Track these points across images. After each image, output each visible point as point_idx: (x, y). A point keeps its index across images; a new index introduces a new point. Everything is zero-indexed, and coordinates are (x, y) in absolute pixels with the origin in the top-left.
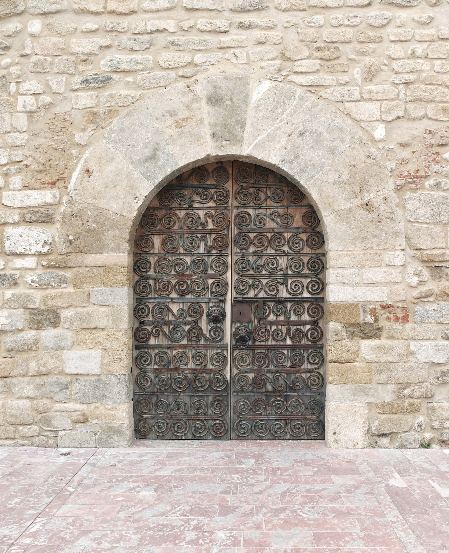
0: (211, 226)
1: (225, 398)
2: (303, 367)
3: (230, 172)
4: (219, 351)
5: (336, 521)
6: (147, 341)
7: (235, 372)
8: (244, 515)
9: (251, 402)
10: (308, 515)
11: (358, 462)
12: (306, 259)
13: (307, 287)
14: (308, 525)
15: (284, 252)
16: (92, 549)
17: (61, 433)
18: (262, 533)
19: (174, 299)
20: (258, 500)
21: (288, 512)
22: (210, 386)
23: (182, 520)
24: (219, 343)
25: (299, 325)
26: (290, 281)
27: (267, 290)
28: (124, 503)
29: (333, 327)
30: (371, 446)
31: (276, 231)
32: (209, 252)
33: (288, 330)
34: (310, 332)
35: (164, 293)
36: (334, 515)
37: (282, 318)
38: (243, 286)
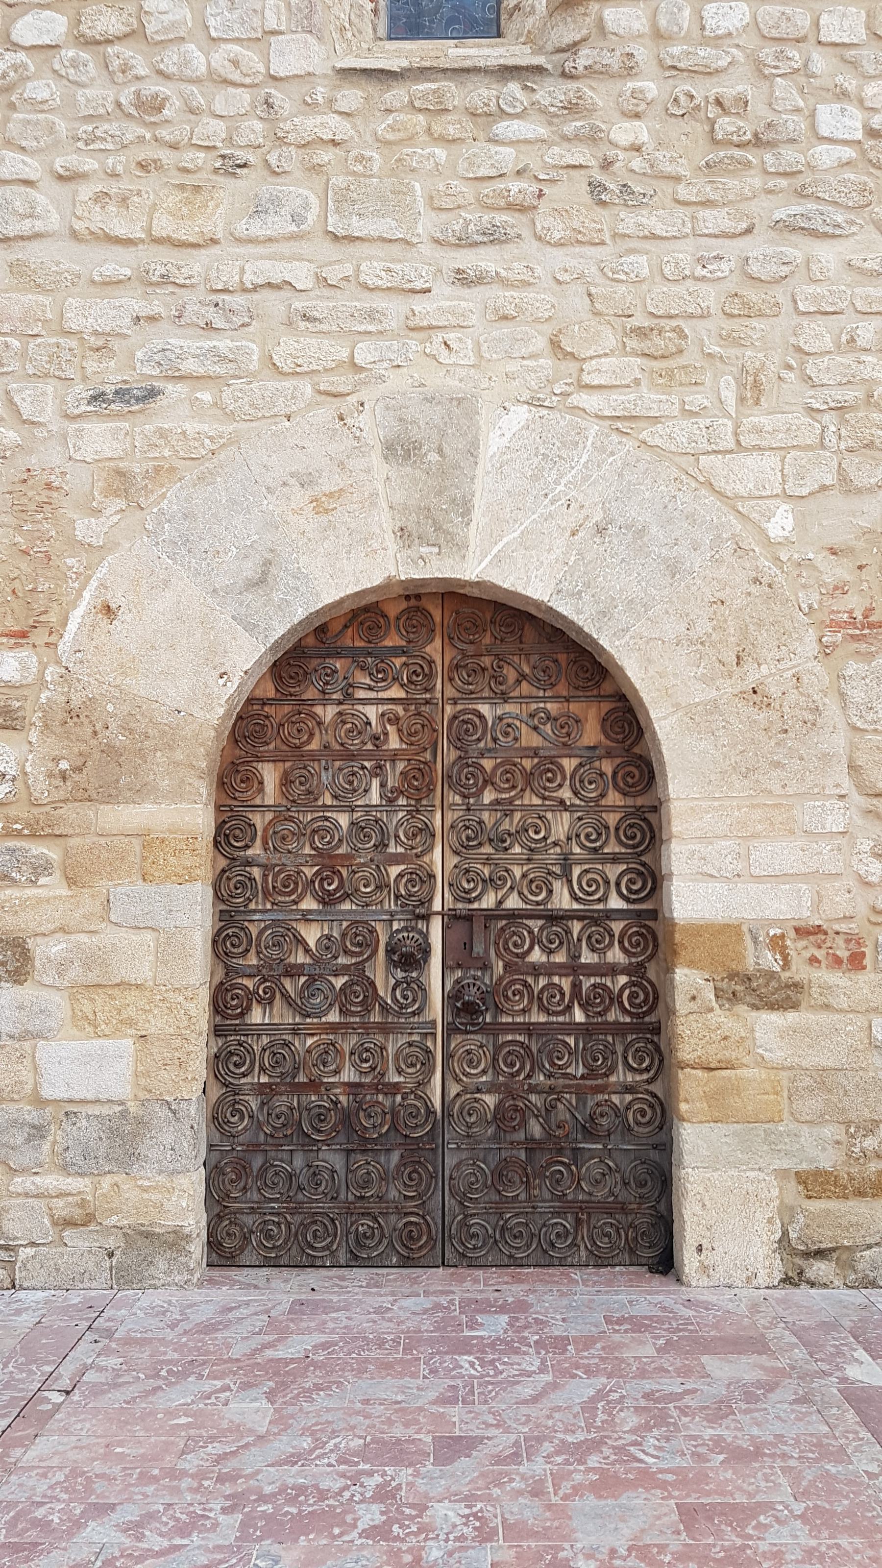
0: (394, 743)
1: (430, 1155)
2: (613, 1079)
3: (438, 619)
4: (415, 1038)
5: (729, 1474)
6: (242, 1015)
7: (454, 1089)
8: (499, 1460)
9: (492, 1167)
10: (657, 1457)
11: (762, 1321)
12: (612, 819)
13: (618, 884)
14: (663, 1485)
15: (562, 802)
16: (122, 1551)
17: (26, 1253)
18: (549, 1507)
19: (310, 912)
20: (528, 1421)
21: (607, 1451)
22: (394, 1127)
23: (343, 1475)
24: (416, 1019)
25: (602, 975)
26: (576, 871)
27: (526, 892)
28: (192, 1432)
29: (687, 980)
30: (787, 1280)
31: (542, 753)
32: (391, 801)
33: (576, 987)
34: (627, 992)
35: (287, 899)
36: (721, 1457)
37: (560, 958)
38: (468, 882)
